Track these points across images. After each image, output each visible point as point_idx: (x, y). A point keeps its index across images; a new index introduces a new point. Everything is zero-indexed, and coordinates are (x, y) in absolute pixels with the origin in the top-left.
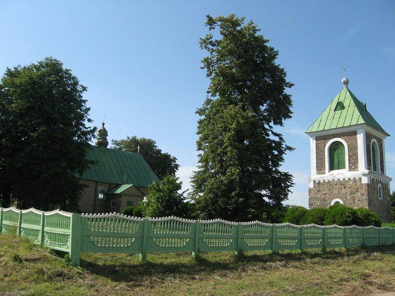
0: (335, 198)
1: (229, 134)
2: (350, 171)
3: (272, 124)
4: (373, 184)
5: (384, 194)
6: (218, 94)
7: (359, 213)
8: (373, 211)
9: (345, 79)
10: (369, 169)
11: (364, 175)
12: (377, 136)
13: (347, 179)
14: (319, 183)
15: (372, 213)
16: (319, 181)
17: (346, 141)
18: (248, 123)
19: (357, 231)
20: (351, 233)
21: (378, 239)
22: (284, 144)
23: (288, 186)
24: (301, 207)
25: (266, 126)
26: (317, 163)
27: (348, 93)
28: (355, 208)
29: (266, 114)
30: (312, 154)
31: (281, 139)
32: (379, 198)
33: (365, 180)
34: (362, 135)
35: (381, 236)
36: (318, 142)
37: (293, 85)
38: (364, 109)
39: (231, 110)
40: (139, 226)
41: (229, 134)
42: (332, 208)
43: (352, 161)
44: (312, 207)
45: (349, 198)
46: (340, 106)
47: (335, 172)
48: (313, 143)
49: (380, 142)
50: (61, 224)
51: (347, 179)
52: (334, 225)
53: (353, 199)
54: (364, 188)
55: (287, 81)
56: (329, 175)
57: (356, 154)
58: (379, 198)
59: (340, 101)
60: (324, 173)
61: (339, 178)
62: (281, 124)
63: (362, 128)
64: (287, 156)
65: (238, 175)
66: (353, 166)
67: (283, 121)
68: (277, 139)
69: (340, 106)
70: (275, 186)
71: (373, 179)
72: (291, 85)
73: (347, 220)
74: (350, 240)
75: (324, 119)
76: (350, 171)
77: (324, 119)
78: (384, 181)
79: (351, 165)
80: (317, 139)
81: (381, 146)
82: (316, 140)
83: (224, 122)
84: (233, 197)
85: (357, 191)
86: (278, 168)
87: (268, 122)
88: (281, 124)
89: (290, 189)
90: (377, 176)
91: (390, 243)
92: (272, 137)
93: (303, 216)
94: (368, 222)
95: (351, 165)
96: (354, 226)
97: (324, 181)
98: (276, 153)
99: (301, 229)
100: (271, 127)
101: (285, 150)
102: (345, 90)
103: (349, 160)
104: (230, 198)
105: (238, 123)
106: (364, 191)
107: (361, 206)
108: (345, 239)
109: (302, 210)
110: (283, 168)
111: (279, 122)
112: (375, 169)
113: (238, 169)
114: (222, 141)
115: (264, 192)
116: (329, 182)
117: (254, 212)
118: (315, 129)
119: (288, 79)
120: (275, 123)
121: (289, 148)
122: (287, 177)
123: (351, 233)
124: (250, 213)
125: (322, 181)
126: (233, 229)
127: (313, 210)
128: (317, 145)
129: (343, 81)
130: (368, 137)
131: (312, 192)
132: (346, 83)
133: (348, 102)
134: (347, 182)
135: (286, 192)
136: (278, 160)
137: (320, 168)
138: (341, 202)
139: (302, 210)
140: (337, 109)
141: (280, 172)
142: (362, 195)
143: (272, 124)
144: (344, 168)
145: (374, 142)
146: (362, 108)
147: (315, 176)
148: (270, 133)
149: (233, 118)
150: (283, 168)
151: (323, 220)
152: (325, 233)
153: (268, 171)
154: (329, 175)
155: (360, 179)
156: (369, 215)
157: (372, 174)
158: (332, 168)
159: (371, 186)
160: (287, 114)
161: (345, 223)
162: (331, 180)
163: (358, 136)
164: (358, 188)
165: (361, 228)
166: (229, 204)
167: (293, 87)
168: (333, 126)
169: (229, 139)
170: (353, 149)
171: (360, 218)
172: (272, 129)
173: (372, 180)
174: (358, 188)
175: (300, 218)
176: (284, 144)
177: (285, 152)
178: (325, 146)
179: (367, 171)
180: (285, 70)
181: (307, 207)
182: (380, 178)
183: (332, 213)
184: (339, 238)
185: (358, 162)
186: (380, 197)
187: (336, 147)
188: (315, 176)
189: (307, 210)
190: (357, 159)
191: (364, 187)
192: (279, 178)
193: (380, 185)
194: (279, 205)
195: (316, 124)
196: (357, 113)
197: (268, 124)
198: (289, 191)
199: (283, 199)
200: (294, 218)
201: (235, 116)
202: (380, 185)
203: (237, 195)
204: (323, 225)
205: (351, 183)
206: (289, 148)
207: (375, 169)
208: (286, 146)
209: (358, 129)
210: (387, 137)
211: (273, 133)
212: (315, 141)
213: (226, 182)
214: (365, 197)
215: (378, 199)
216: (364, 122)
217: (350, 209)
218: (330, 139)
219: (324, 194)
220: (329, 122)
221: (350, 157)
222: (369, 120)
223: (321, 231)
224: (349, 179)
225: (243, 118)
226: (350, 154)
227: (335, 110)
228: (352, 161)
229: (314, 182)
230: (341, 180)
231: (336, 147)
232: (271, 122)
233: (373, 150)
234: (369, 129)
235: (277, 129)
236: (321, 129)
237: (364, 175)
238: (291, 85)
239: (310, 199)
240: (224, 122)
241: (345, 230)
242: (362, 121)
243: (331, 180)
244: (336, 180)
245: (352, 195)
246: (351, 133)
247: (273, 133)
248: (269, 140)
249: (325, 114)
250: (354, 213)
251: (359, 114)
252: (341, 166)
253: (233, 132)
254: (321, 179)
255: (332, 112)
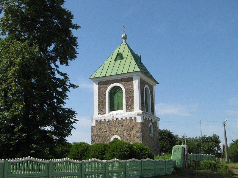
0: (114, 135)
1: (14, 69)
2: (127, 111)
3: (58, 63)
4: (146, 123)
5: (154, 131)
6: (7, 33)
7: (135, 147)
8: (145, 145)
9: (124, 35)
10: (142, 110)
11: (139, 115)
12: (148, 82)
13: (124, 119)
14: (101, 122)
15: (145, 147)
16: (101, 120)
17: (124, 86)
18: (33, 59)
19: (136, 163)
20: (130, 166)
21: (164, 169)
22: (69, 82)
23: (72, 123)
24: (84, 143)
25: (52, 65)
26: (99, 105)
27: (126, 46)
28: (131, 143)
29: (53, 55)
30: (95, 111)
31: (66, 77)
32: (150, 135)
33: (139, 119)
34: (137, 81)
35: (156, 168)
36: (100, 86)
37: (80, 27)
38: (139, 60)
39: (19, 45)
40: (46, 167)
41: (14, 69)
42: (111, 143)
43: (129, 103)
44: (95, 143)
45: (125, 134)
46: (120, 56)
47: (114, 112)
48: (95, 87)
49: (151, 87)
50: (90, 168)
51: (124, 119)
52: (115, 159)
53: (129, 135)
54: (138, 126)
55: (73, 24)
56: (109, 115)
57: (132, 97)
58: (150, 135)
59: (119, 52)
60: (105, 114)
61: (117, 118)
62: (67, 63)
63: (137, 75)
64: (71, 93)
65: (22, 110)
66: (130, 107)
67: (69, 61)
68: (62, 77)
69: (120, 56)
70: (58, 122)
71: (146, 119)
72: (77, 28)
73: (125, 154)
74: (130, 173)
75: (106, 66)
76: (127, 111)
77: (106, 66)
78: (154, 120)
79: (128, 106)
80: (100, 84)
81: (152, 92)
82: (99, 85)
83: (9, 58)
84: (16, 133)
85: (133, 129)
86: (62, 105)
87: (54, 61)
88: (67, 63)
89: (73, 125)
90: (149, 116)
91: (164, 174)
92: (57, 76)
93: (86, 150)
94: (142, 155)
95: (128, 106)
96: (133, 159)
97: (105, 120)
98: (60, 89)
99: (81, 165)
100: (57, 66)
101: (69, 87)
102: (124, 43)
103: (127, 102)
104: (13, 134)
105: (23, 58)
106: (138, 128)
107: (136, 142)
108: (125, 173)
109: (85, 146)
110: (68, 104)
111: (64, 61)
112: (147, 111)
113: (22, 104)
114: (7, 76)
115: (48, 128)
116: (109, 121)
117: (36, 148)
118: (98, 75)
119: (74, 21)
120: (62, 63)
121: (74, 86)
122: (71, 113)
123: (130, 166)
124: (32, 148)
125: (103, 121)
126: (44, 168)
127: (95, 145)
128: (99, 89)
129: (122, 36)
130: (142, 83)
131: (95, 130)
132: (125, 38)
133: (126, 53)
134: (124, 120)
135: (69, 128)
136: (63, 96)
137: (102, 109)
138: (119, 138)
139: (85, 146)
140: (117, 59)
141: (63, 109)
142: (137, 132)
143: (58, 63)
144: (122, 109)
145: (146, 88)
146: (137, 59)
147: (97, 116)
148: (56, 72)
149: (19, 53)
150: (68, 104)
151: (104, 154)
152: (126, 166)
153: (53, 108)
154: (109, 115)
155: (135, 118)
156: (143, 149)
157: (145, 114)
158: (111, 109)
159: (145, 124)
160: (73, 55)
161: (123, 157)
162: (111, 120)
163: (134, 82)
164: (133, 126)
165: (140, 160)
166: (12, 140)
167: (79, 29)
168: (114, 73)
169: (13, 74)
170: (130, 93)
171: (136, 152)
172: (58, 69)
173: (145, 120)
174: (133, 126)
175: (83, 153)
176: (69, 82)
177: (69, 89)
178: (106, 90)
179: (141, 112)
180: (72, 13)
181: (90, 143)
182: (152, 118)
183: (112, 148)
184: (120, 172)
185: (133, 104)
186: (151, 134)
187: (115, 91)
188: (97, 116)
189: (89, 146)
190: (133, 101)
191: (139, 126)
192: (63, 115)
193: (151, 124)
194: (62, 141)
195: (99, 71)
196: (134, 62)
197: (54, 63)
198: (72, 127)
199: (66, 135)
200: (78, 153)
201: (22, 50)
202: (151, 124)
203: (19, 131)
204: (103, 159)
205: (128, 122)
206: (74, 86)
207: (147, 111)
208: (70, 83)
209: (134, 76)
210: (157, 85)
211: (59, 72)
212: (97, 86)
213: (9, 118)
214: (139, 134)
215: (149, 135)
216: (140, 70)
217: (127, 144)
218: (110, 84)
219: (105, 132)
220: (110, 69)
221: (127, 99)
222: (143, 70)
223: (102, 166)
224: (126, 118)
225: (28, 53)
226: (127, 96)
227: (115, 60)
228: (129, 103)
229: (96, 121)
230: (120, 119)
231: (115, 91)
232: (57, 60)
233: (146, 95)
234: (143, 77)
235: (63, 68)
236: (103, 75)
237: (139, 115)
238: (77, 28)
239: (92, 136)
240: (9, 58)
241: (125, 163)
242: (137, 69)
243: (111, 120)
244: (115, 119)
245: (129, 132)
246: (128, 79)
247: (59, 72)
248: (55, 78)
249: (107, 62)
250: (131, 147)
251: (135, 63)
252: (119, 107)
253: (18, 67)
254: (102, 119)
255: (113, 61)
